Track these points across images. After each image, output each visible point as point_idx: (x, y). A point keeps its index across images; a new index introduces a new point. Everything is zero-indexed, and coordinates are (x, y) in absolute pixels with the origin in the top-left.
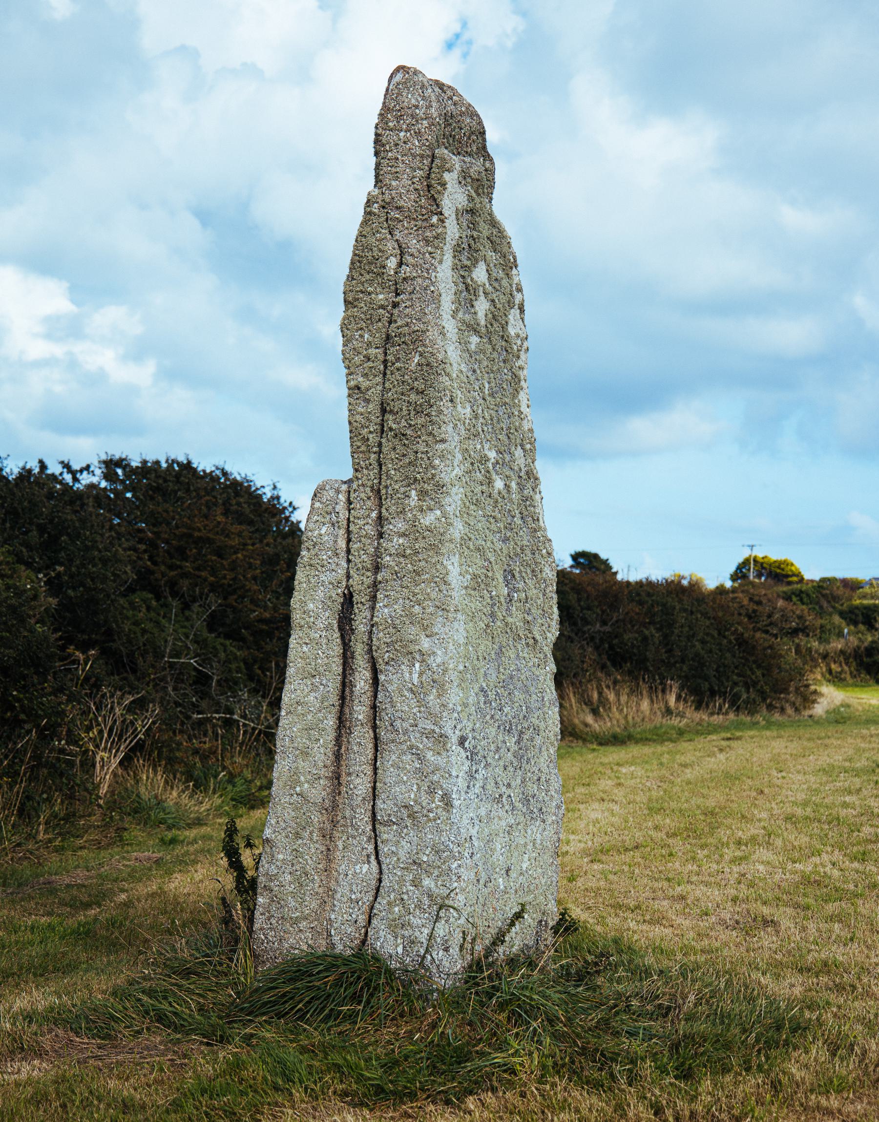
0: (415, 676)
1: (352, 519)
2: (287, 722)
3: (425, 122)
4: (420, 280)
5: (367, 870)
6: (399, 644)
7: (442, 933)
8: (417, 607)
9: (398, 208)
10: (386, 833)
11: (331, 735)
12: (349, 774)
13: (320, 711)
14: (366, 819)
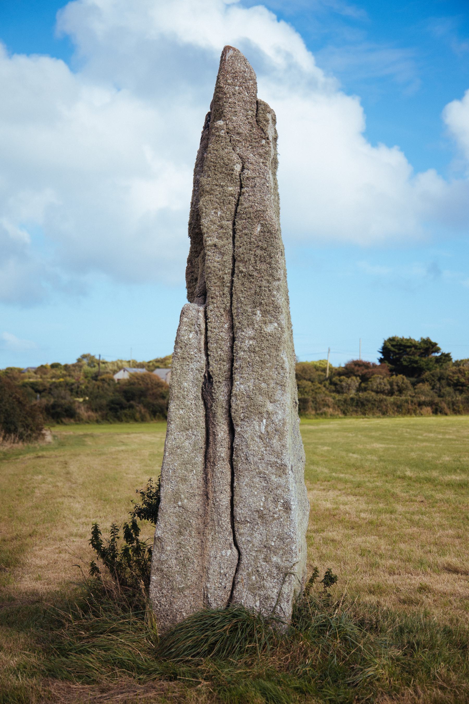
0: (263, 428)
1: (209, 329)
2: (170, 460)
3: (251, 82)
4: (258, 180)
5: (231, 553)
6: (252, 407)
7: (286, 591)
8: (263, 384)
9: (238, 134)
10: (243, 529)
11: (200, 467)
12: (215, 492)
13: (193, 452)
14: (228, 520)
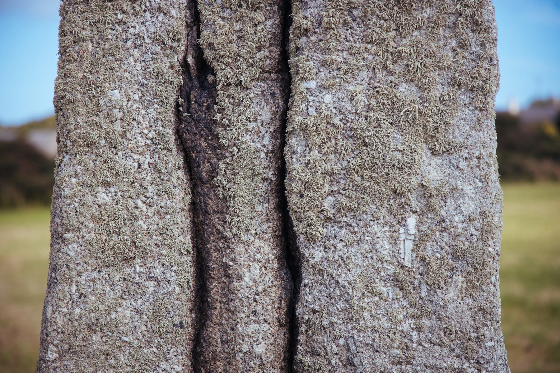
13: (149, 341)
